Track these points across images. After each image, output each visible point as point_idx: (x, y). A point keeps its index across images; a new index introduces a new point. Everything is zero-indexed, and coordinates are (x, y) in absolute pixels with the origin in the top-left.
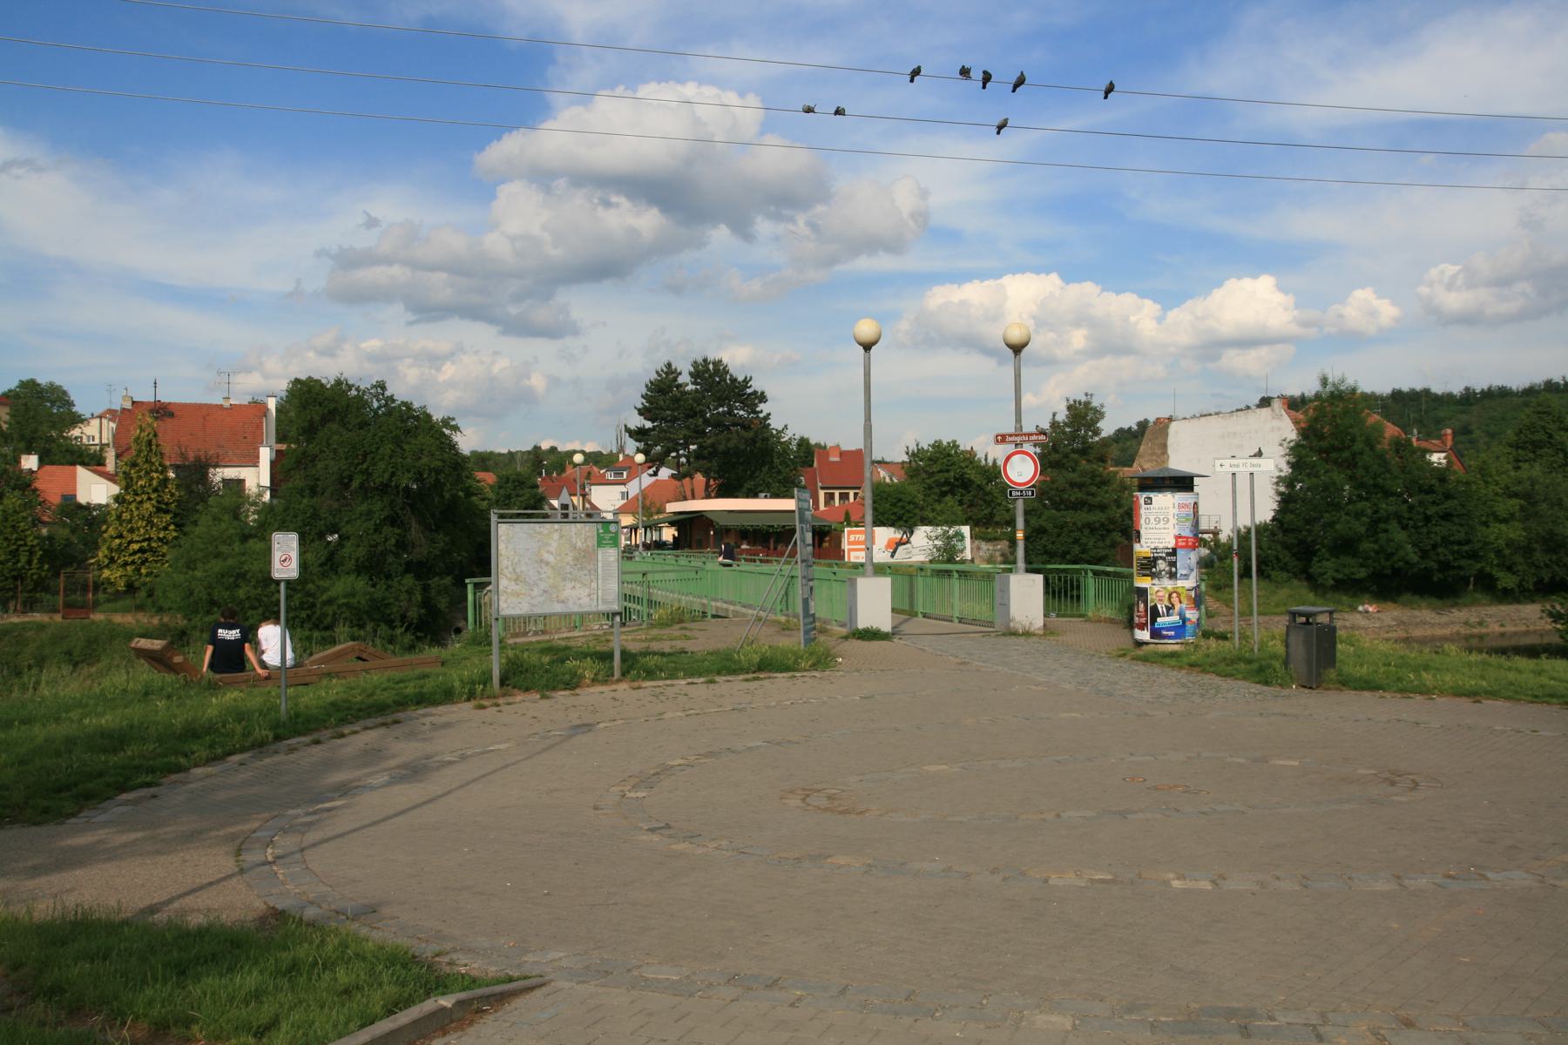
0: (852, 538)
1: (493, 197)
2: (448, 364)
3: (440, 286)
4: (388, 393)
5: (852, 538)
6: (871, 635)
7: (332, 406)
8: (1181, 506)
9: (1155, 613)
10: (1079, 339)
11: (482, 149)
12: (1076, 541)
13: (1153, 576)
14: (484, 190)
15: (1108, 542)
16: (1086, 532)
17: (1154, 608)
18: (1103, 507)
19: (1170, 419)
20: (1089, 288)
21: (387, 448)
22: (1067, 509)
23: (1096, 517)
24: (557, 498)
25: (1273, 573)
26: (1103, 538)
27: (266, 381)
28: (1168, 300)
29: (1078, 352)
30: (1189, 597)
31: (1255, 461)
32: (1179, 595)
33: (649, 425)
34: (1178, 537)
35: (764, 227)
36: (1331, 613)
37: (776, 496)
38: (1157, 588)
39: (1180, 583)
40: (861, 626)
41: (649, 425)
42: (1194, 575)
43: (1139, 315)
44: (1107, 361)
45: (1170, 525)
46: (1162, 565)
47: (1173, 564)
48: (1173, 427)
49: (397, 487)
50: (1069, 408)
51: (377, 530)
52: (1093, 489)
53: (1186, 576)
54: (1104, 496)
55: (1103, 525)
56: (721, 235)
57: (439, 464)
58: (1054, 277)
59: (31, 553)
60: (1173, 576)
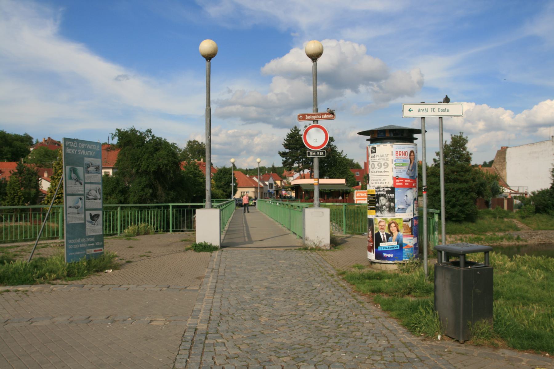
0: (358, 195)
1: (271, 82)
2: (256, 138)
3: (253, 112)
4: (152, 134)
5: (358, 195)
6: (206, 248)
7: (129, 139)
8: (398, 154)
9: (378, 239)
10: (481, 125)
11: (264, 65)
12: (454, 196)
13: (377, 209)
14: (268, 79)
15: (469, 197)
16: (459, 192)
17: (378, 235)
18: (466, 181)
19: (507, 147)
20: (485, 106)
21: (146, 156)
22: (451, 182)
23: (464, 186)
24: (268, 181)
25: (550, 211)
26: (467, 195)
27: (101, 130)
28: (517, 111)
29: (480, 130)
30: (406, 227)
31: (444, 106)
32: (397, 225)
33: (287, 151)
34: (396, 178)
35: (362, 88)
36: (486, 252)
37: (330, 178)
38: (380, 219)
39: (398, 215)
40: (198, 242)
41: (287, 151)
42: (410, 209)
43: (506, 116)
44: (492, 133)
45: (389, 169)
46: (383, 201)
47: (392, 200)
48: (508, 151)
49: (150, 171)
50: (452, 138)
51: (143, 190)
52: (462, 173)
53: (403, 210)
54: (468, 176)
55: (466, 189)
56: (348, 93)
57: (166, 162)
58: (473, 104)
59: (20, 198)
60: (392, 209)
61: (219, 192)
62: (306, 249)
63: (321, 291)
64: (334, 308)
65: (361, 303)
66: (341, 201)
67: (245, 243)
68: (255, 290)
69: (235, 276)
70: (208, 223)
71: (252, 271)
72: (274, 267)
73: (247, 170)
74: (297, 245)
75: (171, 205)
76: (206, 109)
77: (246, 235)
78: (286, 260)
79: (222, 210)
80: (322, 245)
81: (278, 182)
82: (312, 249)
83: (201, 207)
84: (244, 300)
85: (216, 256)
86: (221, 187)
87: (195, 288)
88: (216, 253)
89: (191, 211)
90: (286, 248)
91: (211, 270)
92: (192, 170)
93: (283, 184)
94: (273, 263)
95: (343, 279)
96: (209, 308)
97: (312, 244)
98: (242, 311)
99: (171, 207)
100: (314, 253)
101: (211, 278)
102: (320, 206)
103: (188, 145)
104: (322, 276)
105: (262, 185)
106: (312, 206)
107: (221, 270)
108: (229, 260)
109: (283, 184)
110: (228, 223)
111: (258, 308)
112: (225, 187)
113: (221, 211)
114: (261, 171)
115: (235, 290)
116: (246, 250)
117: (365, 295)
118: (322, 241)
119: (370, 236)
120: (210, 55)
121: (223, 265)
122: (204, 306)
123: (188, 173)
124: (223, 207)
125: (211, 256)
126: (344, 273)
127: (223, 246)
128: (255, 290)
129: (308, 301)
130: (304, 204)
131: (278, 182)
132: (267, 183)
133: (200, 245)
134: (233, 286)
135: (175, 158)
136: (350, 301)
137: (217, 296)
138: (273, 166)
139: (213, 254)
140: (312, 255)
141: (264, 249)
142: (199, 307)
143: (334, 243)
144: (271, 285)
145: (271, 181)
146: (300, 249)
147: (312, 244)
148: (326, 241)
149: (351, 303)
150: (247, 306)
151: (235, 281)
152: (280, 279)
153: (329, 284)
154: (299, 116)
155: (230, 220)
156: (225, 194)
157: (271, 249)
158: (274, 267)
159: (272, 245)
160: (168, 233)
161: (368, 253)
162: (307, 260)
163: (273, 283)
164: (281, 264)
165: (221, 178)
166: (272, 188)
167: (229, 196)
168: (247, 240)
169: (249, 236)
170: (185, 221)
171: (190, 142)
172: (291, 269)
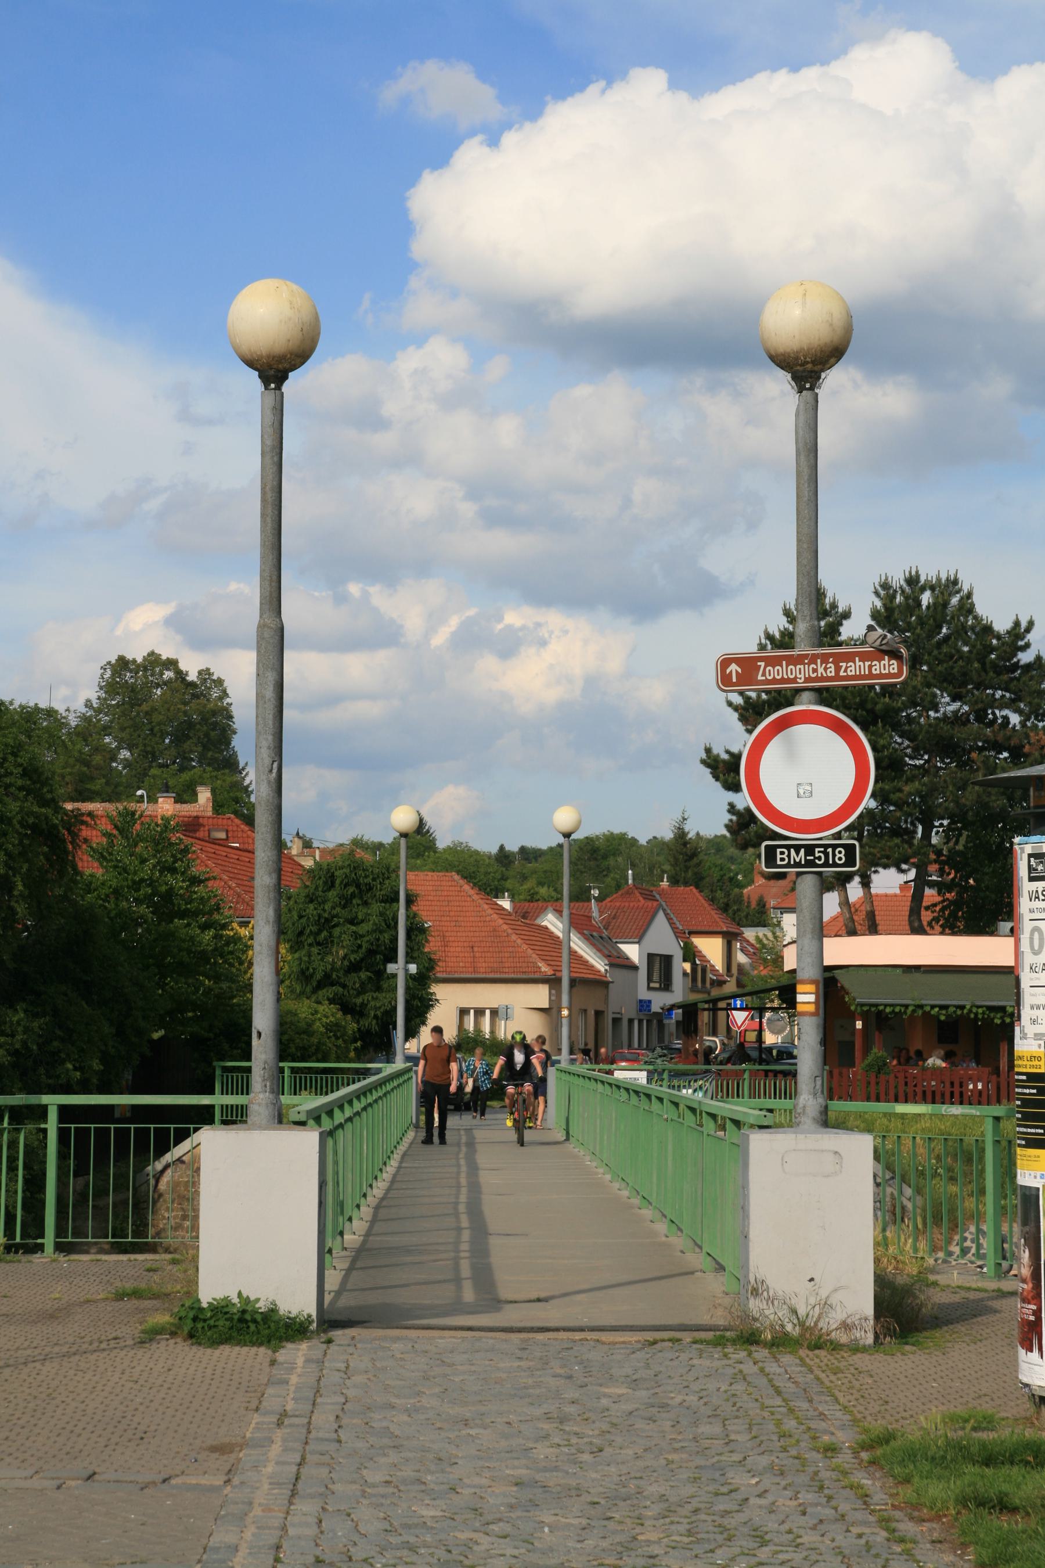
40: (208, 1293)
61: (320, 1012)
62: (750, 1338)
63: (753, 1501)
64: (777, 1552)
65: (902, 1540)
66: (979, 1099)
67: (458, 1307)
68: (466, 1491)
69: (386, 1441)
70: (254, 1198)
71: (466, 1423)
72: (571, 1409)
73: (503, 857)
74: (705, 1319)
75: (52, 1101)
76: (261, 627)
77: (466, 1270)
78: (634, 1383)
79: (331, 1133)
80: (831, 1322)
81: (712, 949)
82: (781, 1342)
83: (235, 1117)
84: (416, 1521)
85: (300, 1361)
86: (327, 981)
87: (205, 1481)
88: (297, 1354)
89: (142, 1135)
90: (650, 1336)
91: (274, 1419)
92: (146, 871)
93: (741, 958)
94: (571, 1394)
95: (872, 1463)
96: (273, 1541)
97: (783, 1313)
98: (405, 1552)
99: (53, 1116)
100: (787, 1359)
101: (276, 1449)
102: (826, 1121)
103: (110, 688)
104: (785, 1450)
105: (599, 964)
106: (789, 1122)
107: (324, 1419)
108: (358, 1379)
109: (741, 958)
110: (366, 1212)
111: (469, 1545)
112: (354, 980)
113: (323, 1137)
114: (597, 866)
115: (382, 1490)
116: (445, 1340)
117: (938, 1518)
118: (833, 1301)
119: (1026, 1272)
120: (281, 358)
121: (329, 1402)
122: (248, 1535)
123: (117, 892)
124: (339, 1117)
125: (273, 1363)
126: (887, 1438)
127: (331, 1321)
128: (466, 1491)
129: (682, 1528)
130: (742, 1108)
131: (712, 949)
132: (632, 951)
133: (221, 1309)
134: (375, 1476)
135: (44, 803)
136: (860, 1536)
137: (306, 1508)
138: (681, 835)
139: (282, 1355)
140: (772, 1368)
141: (540, 1336)
142: (231, 1538)
143: (902, 1313)
144: (539, 1477)
145: (662, 937)
146: (719, 1342)
147: (783, 1313)
148: (859, 1301)
149: (863, 1541)
150: (428, 1538)
151: (383, 1460)
152: (586, 1457)
153: (803, 1479)
154: (725, 662)
155: (379, 1189)
156: (352, 1026)
157: (578, 1336)
158: (571, 1409)
159: (585, 1322)
160: (37, 1258)
161: (1022, 1352)
162: (739, 1387)
163: (556, 1469)
164: (604, 1401)
165: (326, 923)
166: (666, 985)
167: (379, 1043)
168: (469, 1295)
169: (484, 1278)
170: (116, 1194)
171: (123, 663)
172: (652, 1419)
